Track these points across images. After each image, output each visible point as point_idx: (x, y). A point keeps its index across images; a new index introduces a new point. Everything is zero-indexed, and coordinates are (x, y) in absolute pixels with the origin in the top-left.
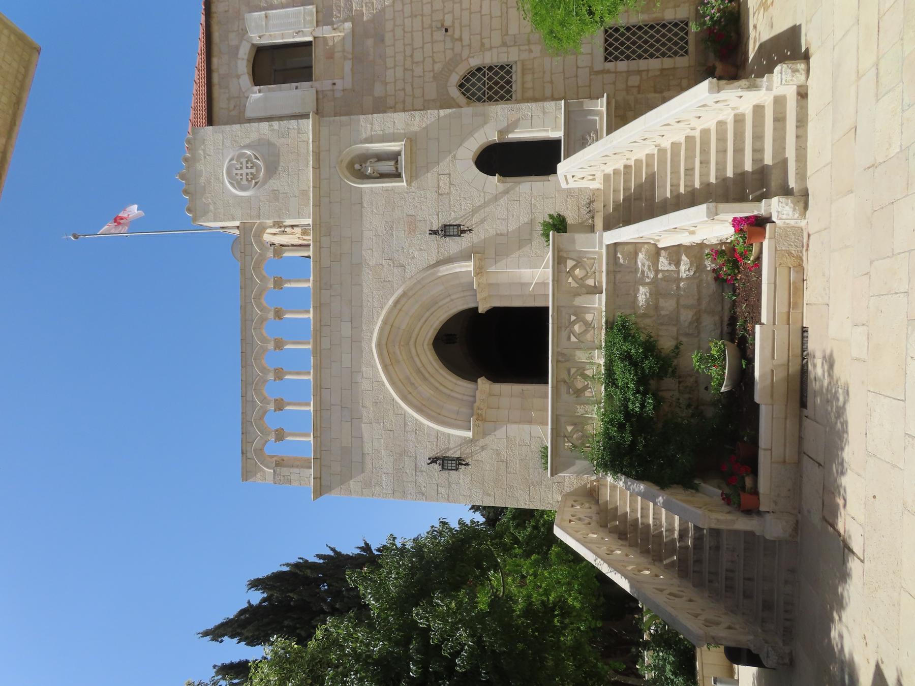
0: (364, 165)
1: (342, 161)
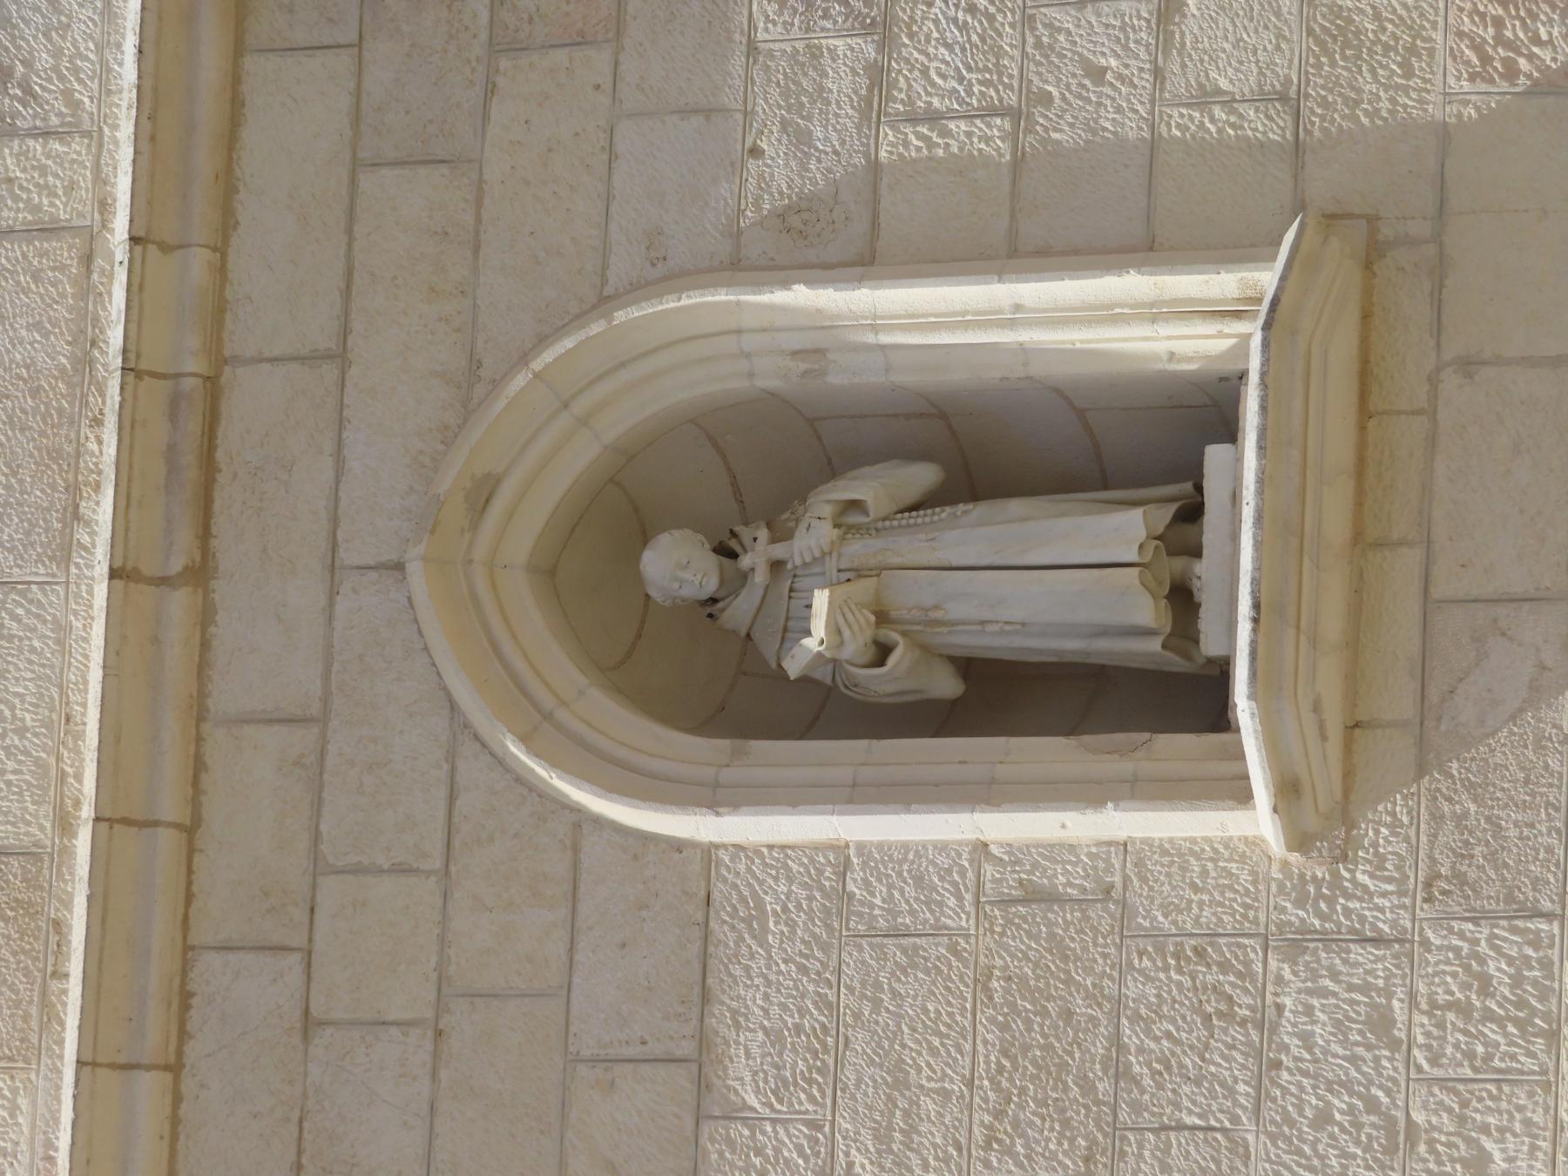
0: (756, 558)
1: (482, 494)
